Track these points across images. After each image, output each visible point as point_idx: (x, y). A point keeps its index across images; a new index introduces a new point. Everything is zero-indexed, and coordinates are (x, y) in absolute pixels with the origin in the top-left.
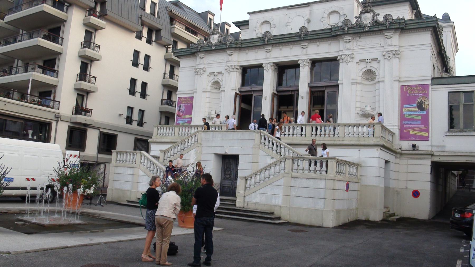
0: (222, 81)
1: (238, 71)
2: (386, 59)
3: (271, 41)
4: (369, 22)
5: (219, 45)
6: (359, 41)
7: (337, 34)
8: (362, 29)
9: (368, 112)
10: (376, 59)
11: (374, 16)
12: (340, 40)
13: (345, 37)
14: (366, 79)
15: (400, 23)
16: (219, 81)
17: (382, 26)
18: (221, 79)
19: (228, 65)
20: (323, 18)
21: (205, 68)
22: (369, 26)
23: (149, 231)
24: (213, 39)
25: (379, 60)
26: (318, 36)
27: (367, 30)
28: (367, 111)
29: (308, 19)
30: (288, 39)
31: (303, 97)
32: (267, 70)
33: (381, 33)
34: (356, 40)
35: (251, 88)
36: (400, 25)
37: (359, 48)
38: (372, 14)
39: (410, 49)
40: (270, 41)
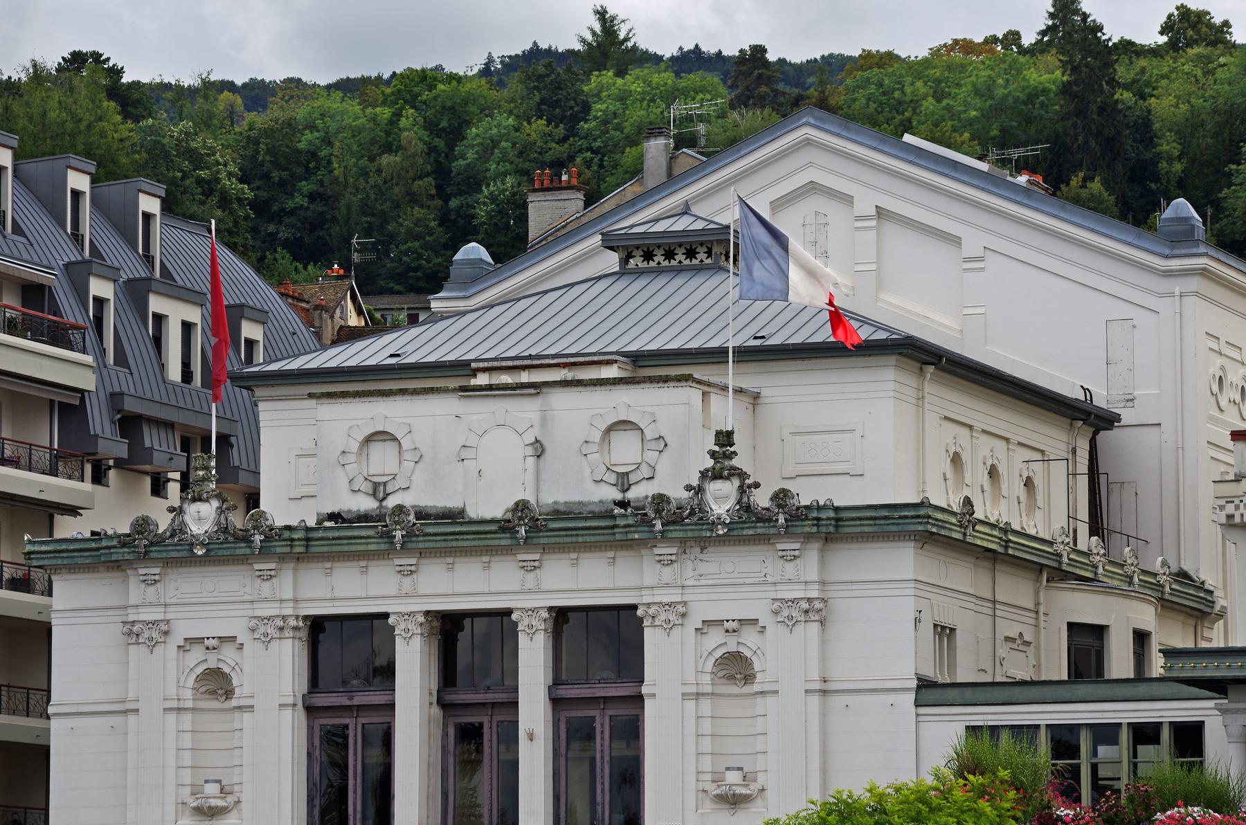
0: (239, 671)
1: (298, 634)
2: (783, 624)
3: (414, 539)
4: (727, 508)
5: (221, 543)
6: (701, 560)
7: (630, 536)
8: (706, 530)
9: (733, 788)
10: (754, 622)
11: (742, 490)
12: (645, 559)
13: (658, 545)
14: (728, 678)
15: (818, 519)
16: (226, 669)
17: (767, 524)
18: (233, 664)
19: (258, 613)
20: (586, 442)
21: (168, 621)
22: (727, 522)
23: (881, 798)
24: (197, 518)
25: (761, 623)
26: (571, 535)
27: (721, 532)
28: (731, 785)
29: (537, 441)
30: (474, 539)
31: (532, 735)
32: (405, 638)
33: (766, 542)
34: (692, 557)
35: (351, 698)
36: (818, 525)
37: (702, 582)
38: (736, 482)
39: (856, 594)
40: (411, 542)
